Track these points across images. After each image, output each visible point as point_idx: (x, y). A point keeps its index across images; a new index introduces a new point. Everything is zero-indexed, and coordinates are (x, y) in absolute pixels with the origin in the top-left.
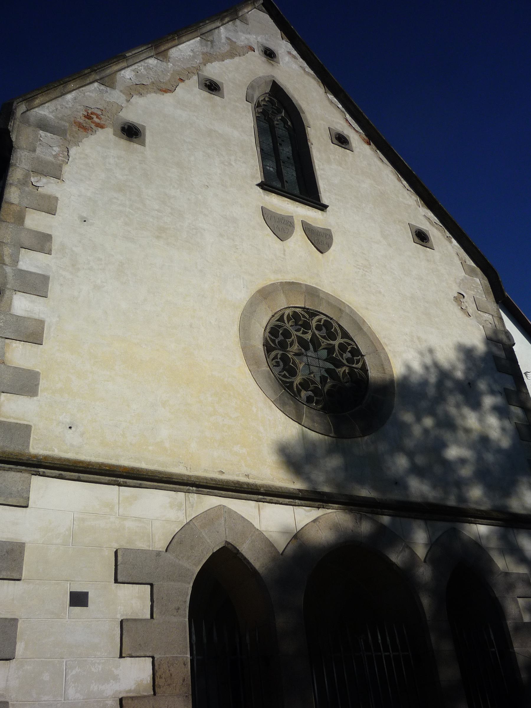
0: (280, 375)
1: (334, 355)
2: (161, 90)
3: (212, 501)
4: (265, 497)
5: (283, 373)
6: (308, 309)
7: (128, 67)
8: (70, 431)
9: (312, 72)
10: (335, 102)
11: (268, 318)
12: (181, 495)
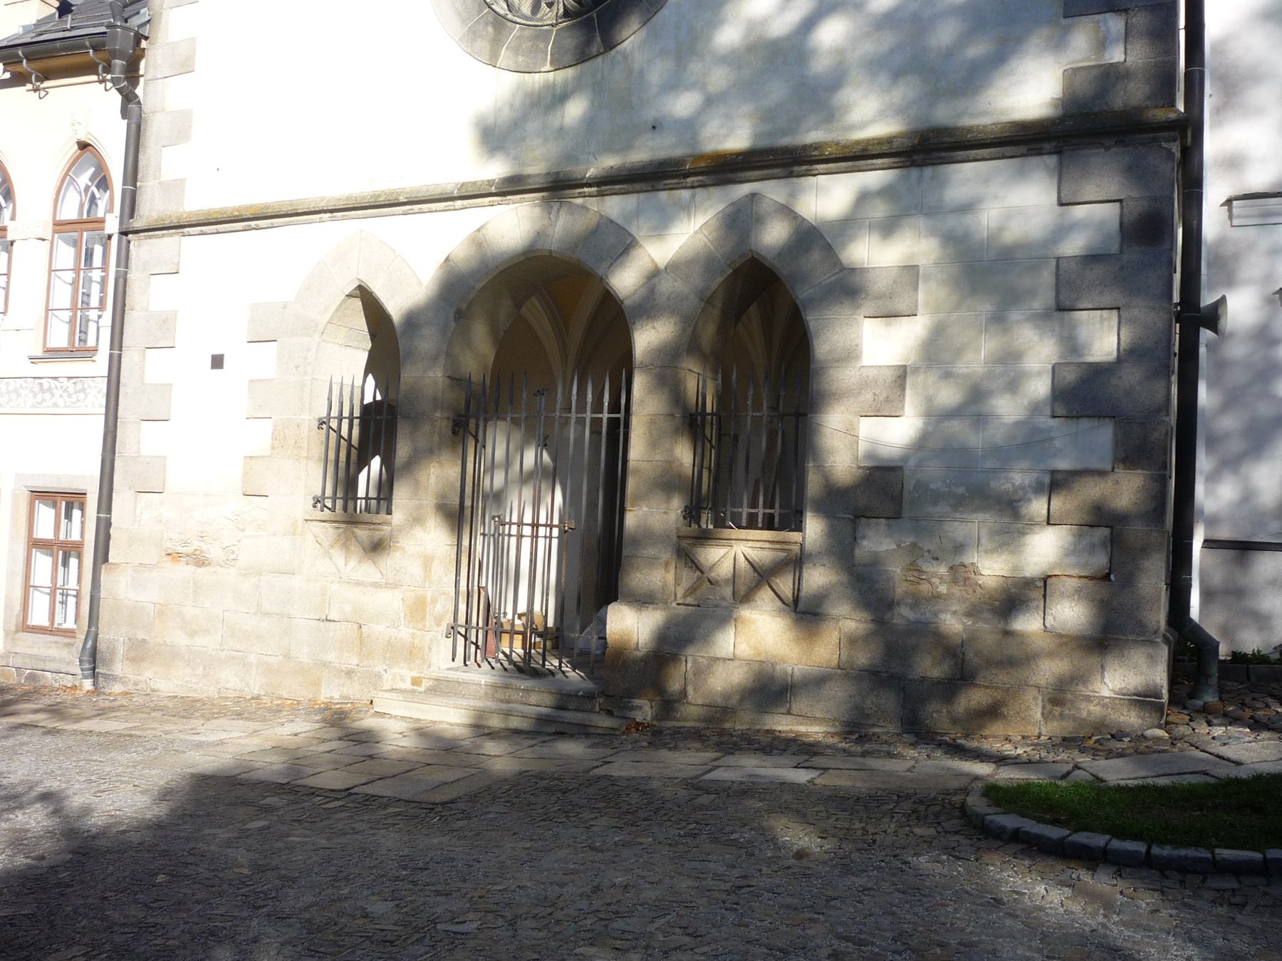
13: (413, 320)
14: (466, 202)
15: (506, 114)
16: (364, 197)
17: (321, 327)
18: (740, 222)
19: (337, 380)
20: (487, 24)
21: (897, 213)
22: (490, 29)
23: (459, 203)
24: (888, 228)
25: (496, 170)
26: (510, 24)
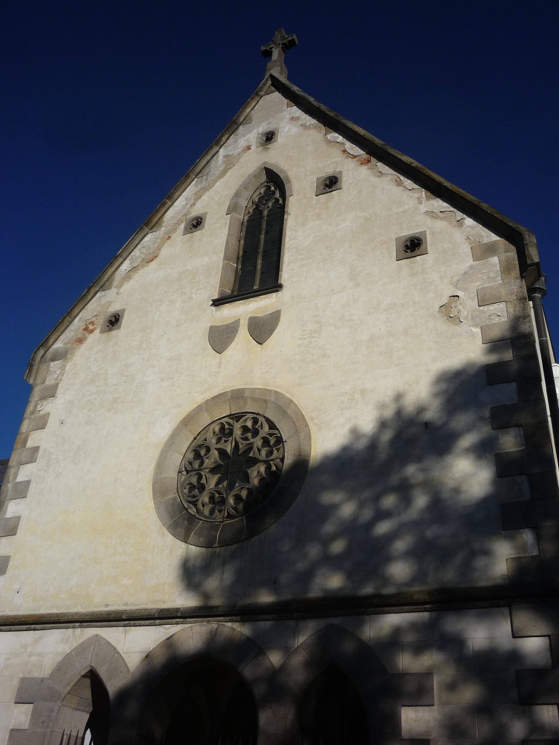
0: (189, 496)
1: (251, 455)
2: (147, 262)
3: (91, 632)
4: (403, 607)
5: (192, 494)
6: (233, 415)
7: (124, 260)
8: (18, 595)
9: (314, 121)
10: (336, 138)
11: (190, 442)
12: (70, 630)
13: (125, 694)
14: (162, 621)
15: (413, 672)
16: (102, 614)
17: (63, 696)
18: (324, 639)
19: (67, 732)
20: (184, 519)
21: (431, 638)
22: (186, 522)
23: (158, 622)
24: (418, 649)
25: (186, 601)
26: (197, 520)
